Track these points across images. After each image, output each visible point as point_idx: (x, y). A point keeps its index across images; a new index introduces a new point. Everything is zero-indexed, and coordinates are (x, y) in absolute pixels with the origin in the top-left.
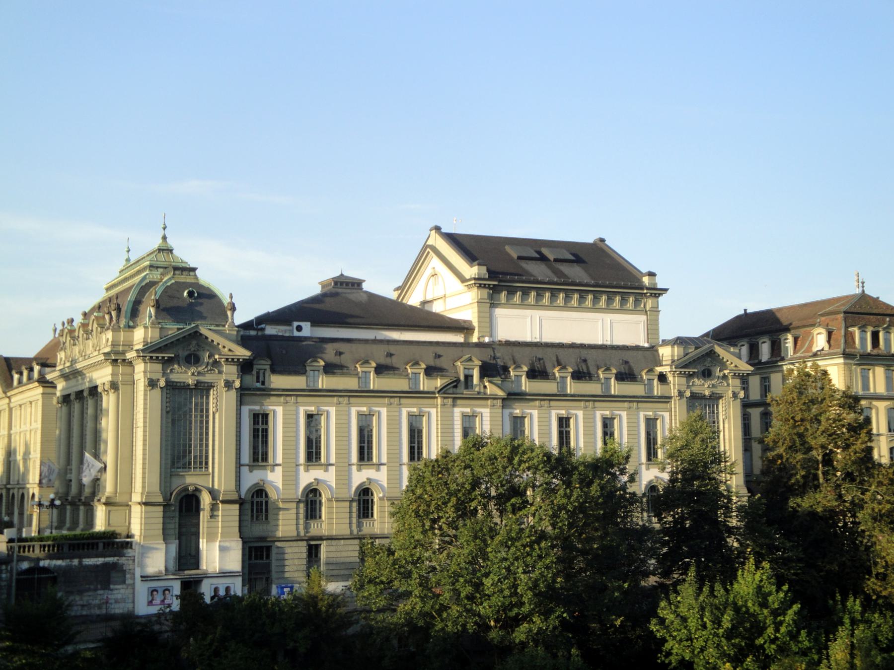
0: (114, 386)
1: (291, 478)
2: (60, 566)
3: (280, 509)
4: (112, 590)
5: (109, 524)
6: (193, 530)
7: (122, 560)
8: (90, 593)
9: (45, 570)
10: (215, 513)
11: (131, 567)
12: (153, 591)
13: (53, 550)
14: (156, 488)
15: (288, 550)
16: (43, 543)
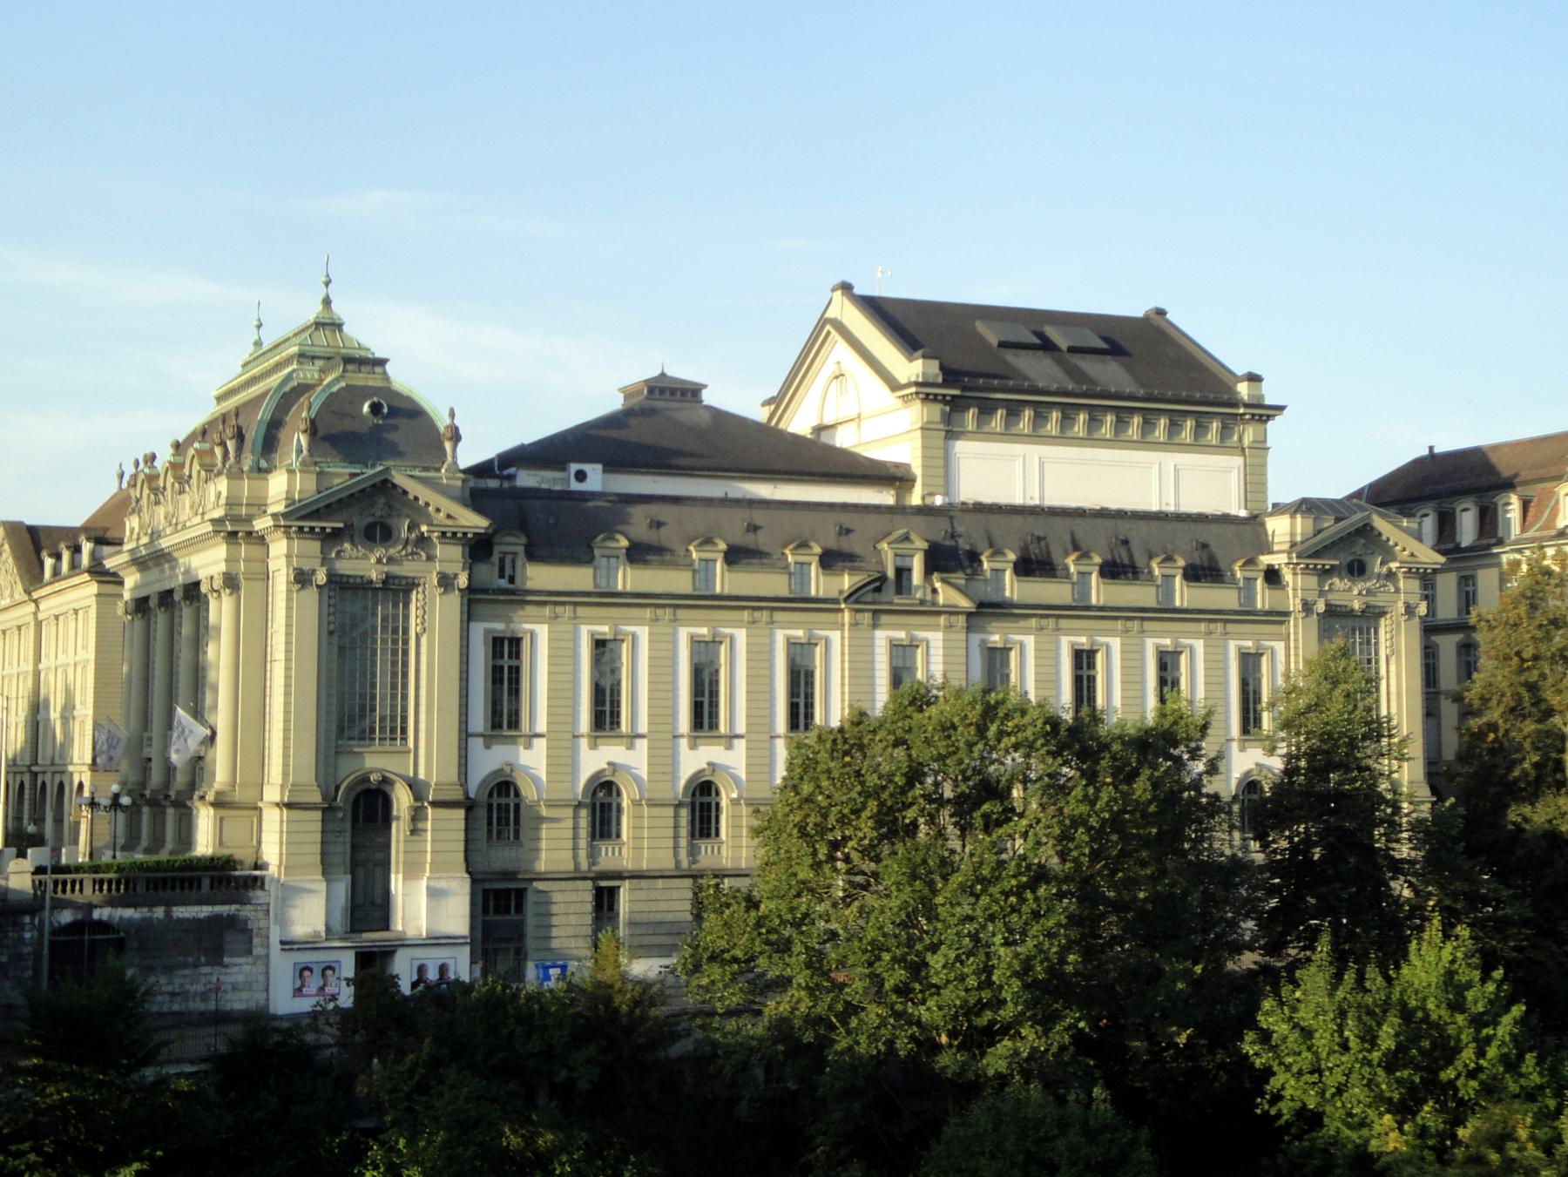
1: (562, 760)
2: (130, 921)
3: (542, 819)
5: (221, 844)
6: (379, 856)
7: (246, 911)
8: (186, 972)
9: (103, 926)
11: (262, 924)
13: (118, 890)
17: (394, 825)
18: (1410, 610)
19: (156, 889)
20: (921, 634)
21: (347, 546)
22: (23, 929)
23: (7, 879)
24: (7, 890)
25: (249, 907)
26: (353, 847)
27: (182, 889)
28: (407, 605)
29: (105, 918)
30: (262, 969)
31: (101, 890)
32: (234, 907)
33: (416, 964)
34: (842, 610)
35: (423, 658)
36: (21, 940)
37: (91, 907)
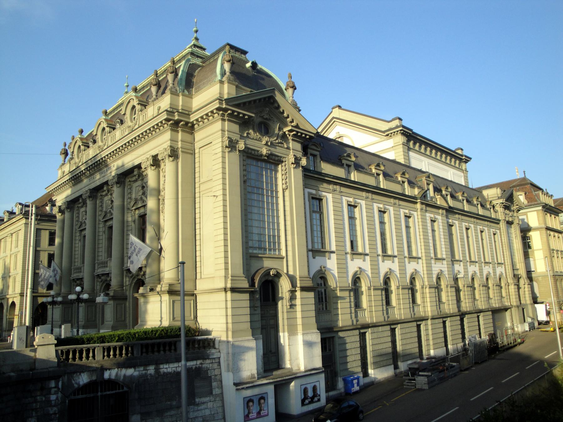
0: (174, 154)
1: (343, 267)
2: (131, 376)
3: (338, 298)
4: (198, 405)
5: (174, 318)
6: (272, 322)
7: (207, 364)
8: (173, 412)
9: (112, 383)
10: (293, 302)
11: (217, 372)
12: (248, 401)
13: (121, 354)
14: (240, 271)
15: (348, 340)
16: (107, 344)
17: (280, 304)
18: (297, 161)
19: (147, 352)
20: (387, 207)
21: (251, 131)
22: (50, 393)
23: (35, 351)
24: (35, 360)
25: (208, 361)
26: (262, 317)
27: (165, 351)
28: (276, 171)
29: (113, 377)
30: (219, 404)
31: (109, 356)
32: (199, 362)
33: (303, 387)
34: (416, 203)
35: (287, 203)
36: (49, 401)
37: (103, 369)
